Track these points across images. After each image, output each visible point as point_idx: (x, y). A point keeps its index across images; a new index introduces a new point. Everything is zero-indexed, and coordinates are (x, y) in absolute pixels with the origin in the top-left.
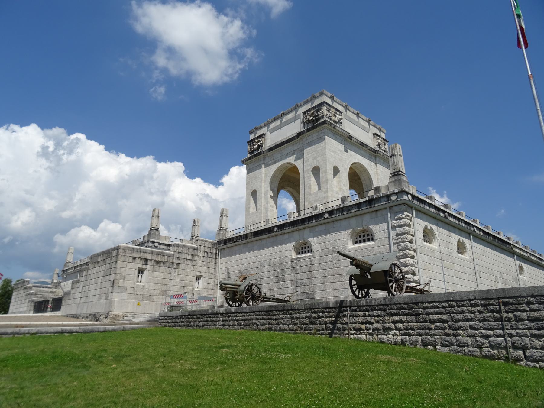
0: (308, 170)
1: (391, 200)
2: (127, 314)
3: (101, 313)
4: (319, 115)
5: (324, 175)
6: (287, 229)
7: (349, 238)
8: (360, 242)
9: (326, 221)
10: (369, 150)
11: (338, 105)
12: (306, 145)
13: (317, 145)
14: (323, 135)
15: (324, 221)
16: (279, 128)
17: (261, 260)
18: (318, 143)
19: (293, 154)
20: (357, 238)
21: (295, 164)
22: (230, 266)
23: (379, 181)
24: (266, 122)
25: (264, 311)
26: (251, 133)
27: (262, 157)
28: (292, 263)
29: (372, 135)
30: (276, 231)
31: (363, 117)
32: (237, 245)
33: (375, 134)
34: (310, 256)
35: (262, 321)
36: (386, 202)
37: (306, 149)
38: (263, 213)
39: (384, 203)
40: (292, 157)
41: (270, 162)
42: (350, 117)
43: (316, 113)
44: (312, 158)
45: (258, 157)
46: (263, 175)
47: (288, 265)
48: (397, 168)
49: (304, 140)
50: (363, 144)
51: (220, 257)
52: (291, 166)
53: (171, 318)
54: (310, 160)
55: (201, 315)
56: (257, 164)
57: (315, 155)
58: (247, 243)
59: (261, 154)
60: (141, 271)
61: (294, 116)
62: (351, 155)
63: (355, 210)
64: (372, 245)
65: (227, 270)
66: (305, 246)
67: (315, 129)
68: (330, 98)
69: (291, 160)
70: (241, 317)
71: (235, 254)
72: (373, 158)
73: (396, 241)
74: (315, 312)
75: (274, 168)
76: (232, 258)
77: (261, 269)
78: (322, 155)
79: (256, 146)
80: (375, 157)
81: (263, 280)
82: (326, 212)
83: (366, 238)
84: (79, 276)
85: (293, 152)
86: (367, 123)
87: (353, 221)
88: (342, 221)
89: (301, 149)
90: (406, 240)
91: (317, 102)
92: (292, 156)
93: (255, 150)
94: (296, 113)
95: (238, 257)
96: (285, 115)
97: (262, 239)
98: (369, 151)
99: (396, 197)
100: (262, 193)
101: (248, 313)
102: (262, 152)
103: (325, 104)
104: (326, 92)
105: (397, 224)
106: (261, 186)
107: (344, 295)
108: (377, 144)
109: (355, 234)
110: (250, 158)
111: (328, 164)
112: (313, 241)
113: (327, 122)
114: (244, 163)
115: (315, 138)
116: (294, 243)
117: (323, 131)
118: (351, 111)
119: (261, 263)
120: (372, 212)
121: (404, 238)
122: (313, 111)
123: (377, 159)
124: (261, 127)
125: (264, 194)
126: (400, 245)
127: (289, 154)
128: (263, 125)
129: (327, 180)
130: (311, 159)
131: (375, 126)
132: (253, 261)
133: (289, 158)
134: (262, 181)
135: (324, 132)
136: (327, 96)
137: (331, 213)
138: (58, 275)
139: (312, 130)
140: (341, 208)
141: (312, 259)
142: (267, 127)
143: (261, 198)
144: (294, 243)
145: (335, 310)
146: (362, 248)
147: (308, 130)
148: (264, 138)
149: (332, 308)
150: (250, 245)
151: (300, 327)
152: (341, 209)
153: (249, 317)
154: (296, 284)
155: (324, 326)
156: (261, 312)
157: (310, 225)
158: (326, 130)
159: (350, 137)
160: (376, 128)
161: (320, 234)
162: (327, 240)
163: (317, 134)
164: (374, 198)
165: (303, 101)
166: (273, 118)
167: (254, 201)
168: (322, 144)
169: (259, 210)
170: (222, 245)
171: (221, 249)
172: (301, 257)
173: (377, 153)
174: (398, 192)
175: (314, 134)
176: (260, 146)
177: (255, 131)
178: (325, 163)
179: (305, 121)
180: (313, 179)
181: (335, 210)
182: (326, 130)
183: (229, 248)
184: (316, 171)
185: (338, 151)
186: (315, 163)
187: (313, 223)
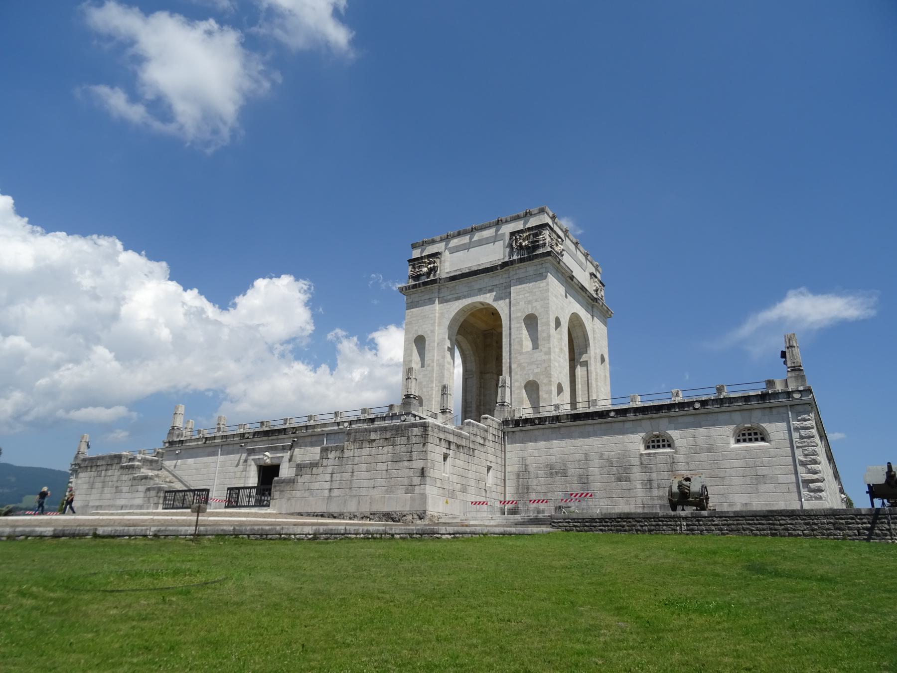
0: (517, 317)
1: (793, 397)
2: (440, 514)
3: (405, 513)
4: (538, 241)
5: (544, 328)
6: (631, 416)
7: (732, 435)
8: (745, 441)
9: (697, 412)
10: (588, 296)
11: (558, 228)
12: (515, 281)
13: (534, 283)
14: (544, 270)
15: (694, 412)
16: (467, 247)
17: (585, 452)
18: (536, 281)
19: (491, 291)
20: (739, 436)
21: (495, 306)
22: (527, 456)
23: (596, 341)
24: (444, 235)
25: (759, 516)
26: (414, 246)
27: (437, 287)
28: (641, 459)
29: (589, 275)
30: (613, 417)
31: (582, 249)
32: (539, 429)
33: (592, 275)
34: (671, 452)
35: (758, 526)
36: (785, 400)
37: (514, 286)
38: (435, 371)
39: (784, 400)
40: (488, 295)
41: (449, 297)
42: (569, 248)
43: (534, 237)
44: (525, 302)
45: (430, 286)
46: (437, 315)
47: (636, 461)
48: (797, 362)
49: (512, 273)
50: (583, 288)
51: (507, 443)
52: (482, 307)
53: (580, 521)
54: (522, 303)
55: (644, 518)
56: (427, 297)
57: (530, 298)
58: (559, 427)
59: (436, 283)
60: (445, 457)
61: (494, 234)
62: (570, 303)
63: (740, 404)
64: (767, 446)
65: (521, 461)
66: (658, 439)
67: (533, 260)
68: (551, 218)
69: (488, 298)
70: (722, 521)
71: (536, 441)
72: (590, 308)
73: (801, 445)
74: (842, 519)
75: (455, 307)
76: (531, 445)
77: (586, 463)
78: (542, 300)
79: (425, 270)
80: (593, 306)
81: (591, 478)
82: (697, 401)
83: (753, 437)
84: (220, 452)
85: (490, 288)
86: (584, 257)
87: (737, 416)
88: (720, 415)
89: (505, 284)
90: (813, 444)
91: (533, 222)
92: (489, 293)
93: (423, 275)
94: (497, 231)
95: (541, 444)
96: (478, 230)
97: (585, 425)
98: (587, 298)
99: (800, 395)
100: (434, 342)
101: (732, 517)
102: (438, 281)
103: (548, 228)
104: (548, 209)
105: (802, 425)
106: (433, 332)
107: (728, 501)
108: (595, 288)
109: (738, 431)
110: (414, 286)
111: (551, 313)
112: (674, 434)
113: (552, 254)
114: (403, 292)
115: (531, 273)
116: (643, 434)
117: (544, 265)
118: (570, 239)
119: (587, 457)
120: (764, 408)
121: (812, 442)
122: (528, 234)
123: (595, 309)
124: (433, 242)
125: (438, 344)
126: (806, 450)
127: (484, 289)
128: (438, 238)
129: (549, 336)
130: (523, 303)
131: (591, 263)
132: (572, 452)
133: (485, 295)
134: (435, 323)
135: (546, 268)
136: (548, 214)
137: (704, 403)
138: (88, 445)
139: (527, 261)
140: (721, 399)
141: (675, 455)
142: (444, 243)
143: (434, 349)
144: (643, 434)
145: (869, 517)
146: (752, 449)
147: (521, 260)
148: (439, 258)
149: (864, 515)
150: (563, 430)
151: (821, 533)
152: (719, 401)
153: (735, 522)
154: (651, 484)
155: (856, 532)
156: (755, 516)
157: (672, 414)
158: (548, 265)
159: (572, 278)
160: (593, 265)
161: (687, 426)
162: (697, 435)
163: (535, 268)
164: (770, 392)
165: (511, 216)
166: (456, 232)
167: (420, 355)
168: (542, 284)
169: (429, 365)
170: (511, 426)
171: (508, 432)
172: (655, 453)
173: (597, 302)
174: (803, 390)
175: (530, 268)
176: (433, 270)
177: (423, 245)
178: (547, 313)
179: (514, 245)
180: (525, 332)
181: (711, 400)
182: (548, 265)
183: (524, 432)
184: (531, 321)
185: (559, 296)
186: (530, 310)
187: (676, 412)
